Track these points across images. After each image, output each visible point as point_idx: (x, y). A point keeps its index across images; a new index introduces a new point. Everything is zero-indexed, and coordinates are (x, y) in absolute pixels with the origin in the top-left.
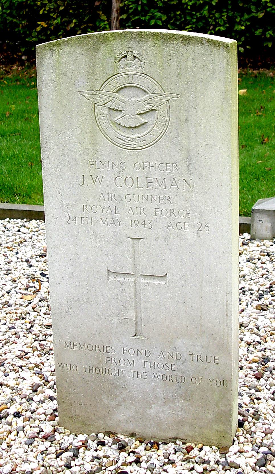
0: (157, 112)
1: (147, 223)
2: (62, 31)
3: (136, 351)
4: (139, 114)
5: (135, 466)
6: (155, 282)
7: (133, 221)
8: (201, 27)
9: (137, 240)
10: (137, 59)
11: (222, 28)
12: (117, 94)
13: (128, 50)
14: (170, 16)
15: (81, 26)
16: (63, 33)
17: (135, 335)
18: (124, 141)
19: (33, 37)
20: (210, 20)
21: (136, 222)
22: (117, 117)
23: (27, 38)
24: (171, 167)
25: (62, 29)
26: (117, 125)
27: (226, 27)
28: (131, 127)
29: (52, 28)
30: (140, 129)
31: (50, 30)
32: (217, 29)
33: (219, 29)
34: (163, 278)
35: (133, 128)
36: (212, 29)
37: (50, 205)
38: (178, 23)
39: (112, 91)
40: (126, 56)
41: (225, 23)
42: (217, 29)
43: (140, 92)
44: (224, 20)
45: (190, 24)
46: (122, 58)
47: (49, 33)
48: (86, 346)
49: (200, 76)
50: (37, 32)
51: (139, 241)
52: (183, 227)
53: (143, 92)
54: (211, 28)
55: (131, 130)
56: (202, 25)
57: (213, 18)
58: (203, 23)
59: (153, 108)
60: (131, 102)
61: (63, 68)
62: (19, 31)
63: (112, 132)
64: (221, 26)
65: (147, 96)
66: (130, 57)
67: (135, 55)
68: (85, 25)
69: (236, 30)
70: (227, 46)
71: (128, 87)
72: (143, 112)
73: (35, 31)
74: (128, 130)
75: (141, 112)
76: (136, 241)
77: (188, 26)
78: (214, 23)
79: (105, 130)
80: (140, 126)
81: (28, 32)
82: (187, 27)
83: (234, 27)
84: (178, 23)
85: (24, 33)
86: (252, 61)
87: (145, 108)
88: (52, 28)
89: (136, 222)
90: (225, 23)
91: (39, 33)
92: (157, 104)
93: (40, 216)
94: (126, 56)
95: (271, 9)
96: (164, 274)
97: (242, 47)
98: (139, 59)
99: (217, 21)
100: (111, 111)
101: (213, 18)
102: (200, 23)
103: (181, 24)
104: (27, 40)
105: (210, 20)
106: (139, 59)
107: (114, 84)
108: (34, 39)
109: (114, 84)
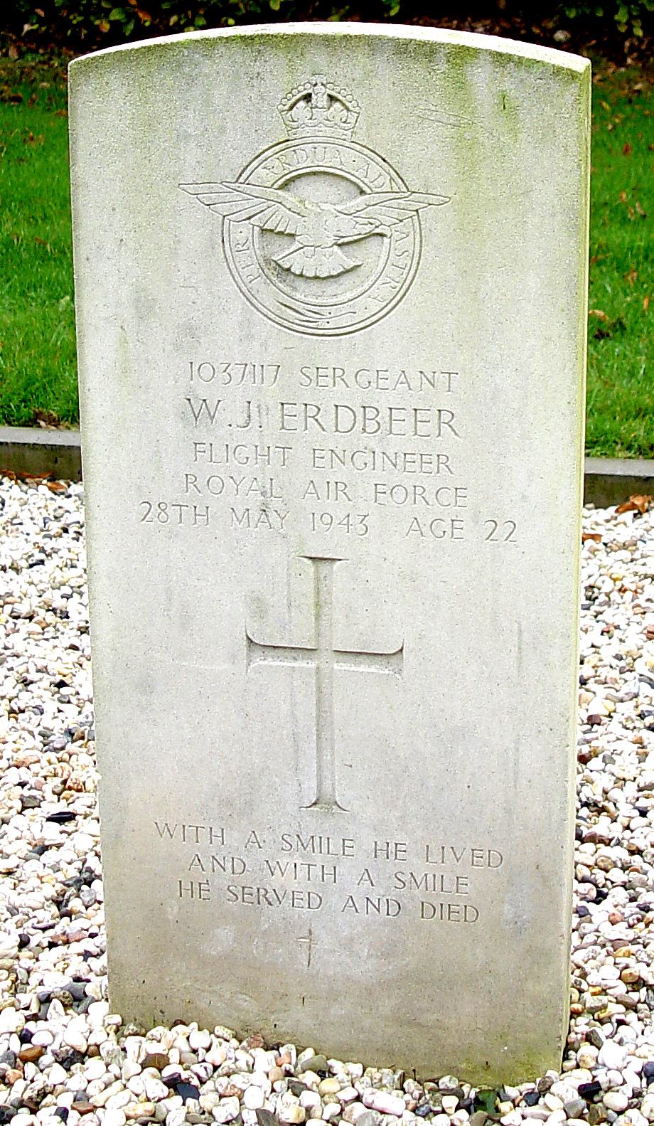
3: (348, 460)
4: (339, 245)
5: (207, 402)
6: (353, 668)
10: (337, 105)
12: (279, 192)
17: (315, 804)
18: (301, 314)
21: (327, 519)
30: (345, 280)
34: (394, 660)
35: (324, 278)
37: (97, 436)
40: (308, 98)
55: (316, 284)
59: (377, 231)
61: (146, 137)
66: (320, 99)
67: (333, 94)
70: (573, 75)
71: (315, 173)
75: (346, 240)
76: (324, 568)
87: (351, 230)
89: (327, 519)
92: (388, 221)
93: (61, 467)
94: (308, 98)
98: (343, 104)
106: (343, 104)
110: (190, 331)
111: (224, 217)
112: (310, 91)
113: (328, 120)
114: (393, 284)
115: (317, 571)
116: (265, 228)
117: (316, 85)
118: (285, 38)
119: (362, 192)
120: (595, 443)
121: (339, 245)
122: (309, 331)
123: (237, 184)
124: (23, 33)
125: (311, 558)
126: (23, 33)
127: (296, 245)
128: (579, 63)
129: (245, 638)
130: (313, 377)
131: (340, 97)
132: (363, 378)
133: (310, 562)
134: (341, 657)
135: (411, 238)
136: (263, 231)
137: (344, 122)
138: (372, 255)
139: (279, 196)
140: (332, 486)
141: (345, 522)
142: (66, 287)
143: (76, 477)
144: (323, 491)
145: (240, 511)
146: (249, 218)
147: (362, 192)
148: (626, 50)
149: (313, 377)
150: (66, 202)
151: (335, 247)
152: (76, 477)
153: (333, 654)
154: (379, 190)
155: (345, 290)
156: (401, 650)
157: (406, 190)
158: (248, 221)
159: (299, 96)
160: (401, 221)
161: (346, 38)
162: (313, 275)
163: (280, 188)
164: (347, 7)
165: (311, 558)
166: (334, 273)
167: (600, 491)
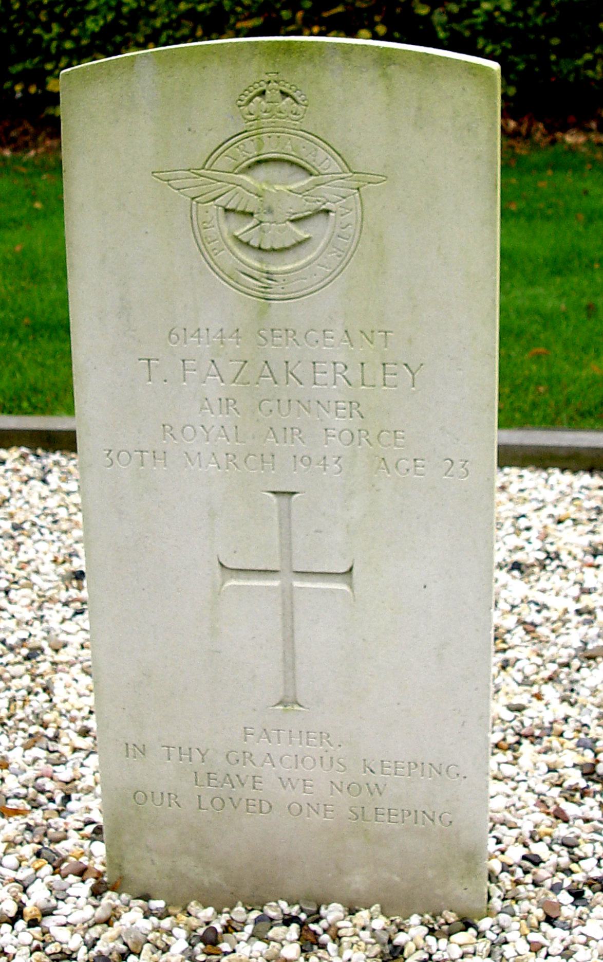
4: (292, 221)
6: (314, 586)
7: (298, 459)
9: (288, 496)
10: (288, 99)
12: (241, 176)
13: (267, 78)
14: (38, 88)
18: (257, 280)
22: (243, 229)
24: (284, 337)
28: (274, 250)
37: (93, 409)
39: (231, 170)
40: (263, 93)
43: (287, 170)
48: (299, 760)
49: (423, 127)
51: (290, 499)
59: (324, 207)
61: (134, 129)
67: (283, 89)
72: (301, 215)
74: (255, 254)
75: (297, 216)
76: (284, 499)
80: (294, 246)
86: (535, 108)
87: (303, 206)
93: (64, 442)
94: (263, 93)
98: (294, 99)
100: (232, 216)
106: (294, 99)
107: (249, 151)
111: (193, 199)
113: (280, 112)
114: (340, 253)
116: (228, 207)
117: (269, 82)
119: (311, 175)
121: (292, 221)
123: (202, 171)
124: (43, 116)
125: (274, 493)
126: (43, 116)
128: (495, 66)
129: (217, 565)
130: (270, 338)
133: (271, 495)
134: (298, 576)
135: (354, 211)
136: (226, 210)
137: (295, 114)
138: (316, 229)
140: (289, 431)
143: (74, 449)
144: (280, 434)
146: (214, 200)
148: (326, 15)
149: (270, 338)
150: (61, 201)
151: (288, 223)
152: (74, 449)
154: (326, 171)
156: (351, 569)
158: (212, 203)
159: (255, 92)
160: (344, 198)
165: (274, 493)
166: (276, 247)
167: (510, 457)
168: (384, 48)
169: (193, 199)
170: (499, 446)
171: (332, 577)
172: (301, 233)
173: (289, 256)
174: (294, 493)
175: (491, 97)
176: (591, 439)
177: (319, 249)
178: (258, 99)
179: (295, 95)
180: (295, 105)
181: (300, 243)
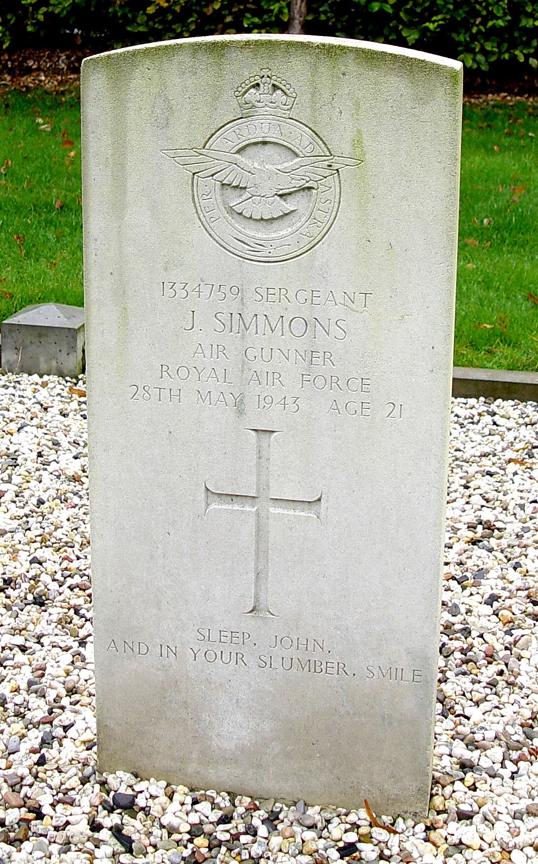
0: (314, 191)
1: (289, 401)
2: (195, 15)
4: (281, 196)
6: (286, 512)
8: (462, 19)
9: (267, 434)
10: (279, 92)
11: (500, 23)
15: (233, 6)
16: (197, 19)
19: (139, 25)
20: (478, 7)
23: (130, 26)
25: (196, 11)
26: (236, 216)
27: (508, 21)
28: (273, 219)
29: (177, 9)
31: (174, 12)
32: (490, 24)
33: (494, 25)
34: (315, 507)
36: (481, 23)
38: (418, 10)
40: (258, 85)
41: (505, 14)
42: (490, 24)
44: (504, 9)
45: (441, 13)
46: (250, 88)
47: (170, 17)
49: (392, 130)
50: (148, 15)
52: (359, 411)
53: (288, 153)
54: (478, 20)
56: (464, 15)
57: (484, 4)
58: (465, 12)
59: (307, 185)
60: (267, 171)
61: (149, 120)
62: (116, 12)
63: (229, 228)
64: (498, 18)
65: (295, 161)
68: (242, 7)
69: (525, 26)
70: (453, 73)
72: (287, 191)
73: (145, 13)
74: (260, 225)
76: (265, 436)
77: (436, 15)
78: (484, 13)
79: (212, 225)
80: (281, 217)
81: (129, 15)
82: (434, 18)
83: (520, 21)
84: (418, 10)
85: (124, 15)
88: (177, 9)
89: (268, 400)
90: (505, 14)
91: (150, 17)
94: (258, 85)
95: (477, 22)
96: (316, 498)
97: (534, 58)
99: (490, 9)
100: (229, 191)
101: (484, 4)
102: (461, 12)
103: (424, 11)
104: (129, 29)
105: (478, 7)
108: (141, 29)
109: (230, 138)
110: (517, 536)
111: (194, 174)
112: (259, 81)
115: (259, 441)
118: (406, 59)
119: (297, 156)
120: (72, 334)
122: (258, 259)
127: (247, 195)
129: (204, 488)
130: (265, 295)
131: (281, 86)
132: (302, 296)
133: (253, 432)
139: (236, 159)
140: (215, 347)
141: (282, 402)
142: (78, 228)
145: (204, 393)
146: (213, 175)
147: (297, 156)
153: (272, 502)
155: (283, 230)
156: (319, 500)
157: (328, 154)
161: (384, 54)
162: (259, 217)
163: (238, 152)
164: (92, 9)
168: (374, 40)
169: (194, 174)
170: (454, 379)
171: (281, 503)
172: (288, 206)
173: (276, 224)
174: (273, 432)
175: (453, 105)
176: (531, 378)
177: (236, 225)
178: (252, 90)
179: (283, 88)
180: (284, 97)
181: (293, 211)
